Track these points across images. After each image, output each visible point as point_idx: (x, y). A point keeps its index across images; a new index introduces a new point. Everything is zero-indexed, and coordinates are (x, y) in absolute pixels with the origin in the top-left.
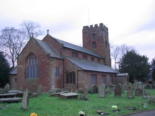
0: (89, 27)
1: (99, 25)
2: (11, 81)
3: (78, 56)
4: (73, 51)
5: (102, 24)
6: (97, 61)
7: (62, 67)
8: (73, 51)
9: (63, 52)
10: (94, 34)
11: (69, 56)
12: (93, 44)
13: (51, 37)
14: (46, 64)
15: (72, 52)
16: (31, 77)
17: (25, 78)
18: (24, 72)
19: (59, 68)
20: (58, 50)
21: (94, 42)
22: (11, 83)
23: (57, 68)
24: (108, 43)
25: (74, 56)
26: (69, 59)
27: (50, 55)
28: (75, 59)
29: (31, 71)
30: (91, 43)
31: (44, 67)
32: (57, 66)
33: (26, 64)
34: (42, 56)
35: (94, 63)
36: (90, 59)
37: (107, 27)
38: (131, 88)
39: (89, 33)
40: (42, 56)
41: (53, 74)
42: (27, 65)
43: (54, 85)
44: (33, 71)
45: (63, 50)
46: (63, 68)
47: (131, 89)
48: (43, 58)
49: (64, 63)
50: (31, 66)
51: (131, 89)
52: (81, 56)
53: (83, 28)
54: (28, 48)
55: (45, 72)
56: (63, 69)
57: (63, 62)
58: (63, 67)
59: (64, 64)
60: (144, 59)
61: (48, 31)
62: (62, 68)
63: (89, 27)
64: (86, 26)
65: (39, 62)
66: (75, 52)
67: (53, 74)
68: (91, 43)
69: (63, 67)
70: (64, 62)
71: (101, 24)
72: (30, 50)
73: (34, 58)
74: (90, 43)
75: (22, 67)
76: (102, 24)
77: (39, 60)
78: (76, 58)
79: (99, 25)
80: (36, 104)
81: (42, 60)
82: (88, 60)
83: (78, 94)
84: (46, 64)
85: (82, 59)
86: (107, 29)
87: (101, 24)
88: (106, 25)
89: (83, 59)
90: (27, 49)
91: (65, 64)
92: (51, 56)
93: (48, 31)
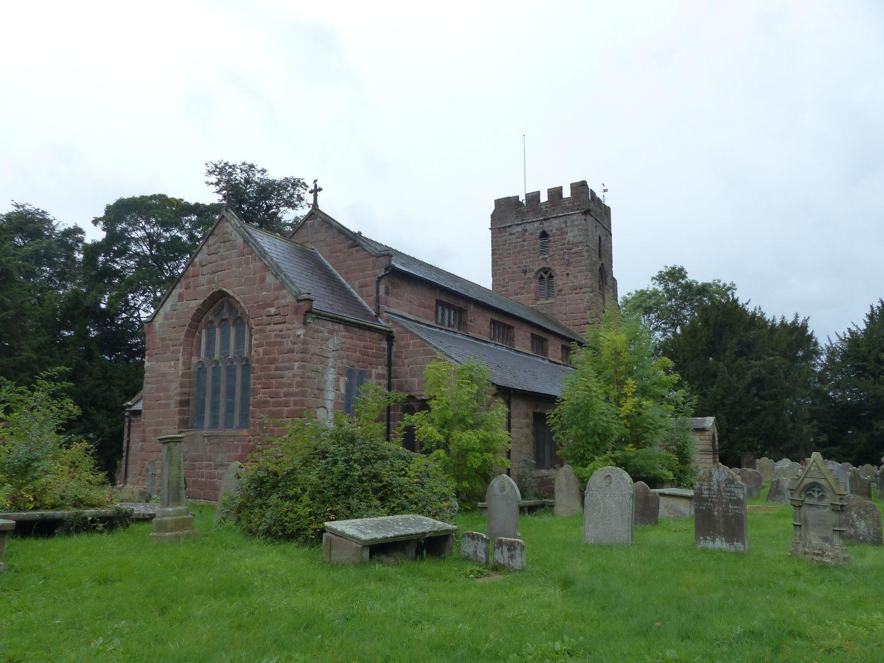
0: (522, 198)
1: (567, 193)
2: (128, 447)
3: (465, 324)
4: (444, 298)
5: (584, 184)
6: (560, 354)
7: (381, 370)
8: (444, 298)
9: (387, 293)
10: (544, 235)
11: (421, 320)
12: (542, 278)
13: (328, 223)
14: (291, 351)
15: (439, 303)
16: (214, 424)
17: (179, 427)
18: (178, 398)
19: (363, 376)
20: (361, 287)
21: (546, 270)
22: (130, 459)
23: (355, 377)
24: (609, 277)
25: (446, 323)
26: (416, 332)
27: (311, 300)
28: (451, 334)
29: (216, 392)
30: (531, 275)
31: (281, 365)
32: (352, 363)
33: (191, 355)
34: (272, 310)
35: (547, 362)
36: (528, 343)
37: (607, 204)
38: (828, 494)
39: (519, 229)
40: (272, 310)
41: (329, 405)
42: (195, 360)
43: (692, 480)
44: (223, 389)
45: (386, 287)
46: (390, 377)
47: (822, 497)
48: (278, 319)
49: (394, 349)
50: (217, 363)
51: (826, 502)
52: (481, 323)
53: (492, 208)
54: (205, 270)
55: (286, 394)
56: (385, 382)
57: (384, 345)
58: (386, 373)
59: (393, 358)
60: (797, 336)
61: (315, 181)
62: (379, 376)
63: (522, 198)
64: (508, 200)
65: (253, 342)
66: (449, 299)
67: (329, 405)
68: (531, 275)
69: (389, 371)
70: (390, 345)
71: (580, 188)
72: (210, 282)
73: (231, 322)
74: (527, 276)
75: (170, 367)
76: (584, 184)
77: (257, 332)
78: (456, 330)
79: (567, 193)
80: (76, 620)
81: (269, 328)
82: (517, 348)
83: (450, 526)
84: (291, 351)
85: (488, 340)
86: (607, 210)
87: (580, 188)
88: (599, 195)
89: (493, 339)
90: (196, 276)
91: (396, 356)
92: (316, 305)
93: (315, 181)
